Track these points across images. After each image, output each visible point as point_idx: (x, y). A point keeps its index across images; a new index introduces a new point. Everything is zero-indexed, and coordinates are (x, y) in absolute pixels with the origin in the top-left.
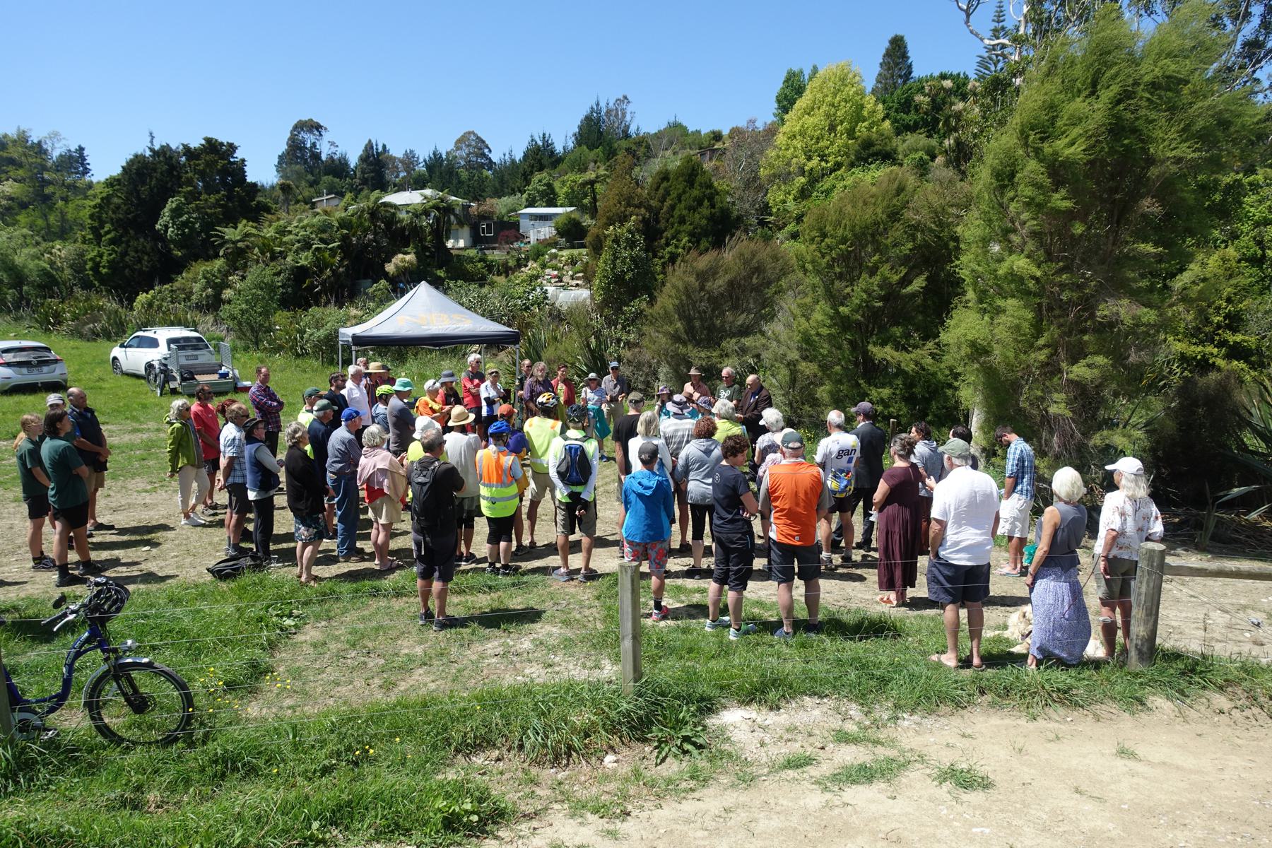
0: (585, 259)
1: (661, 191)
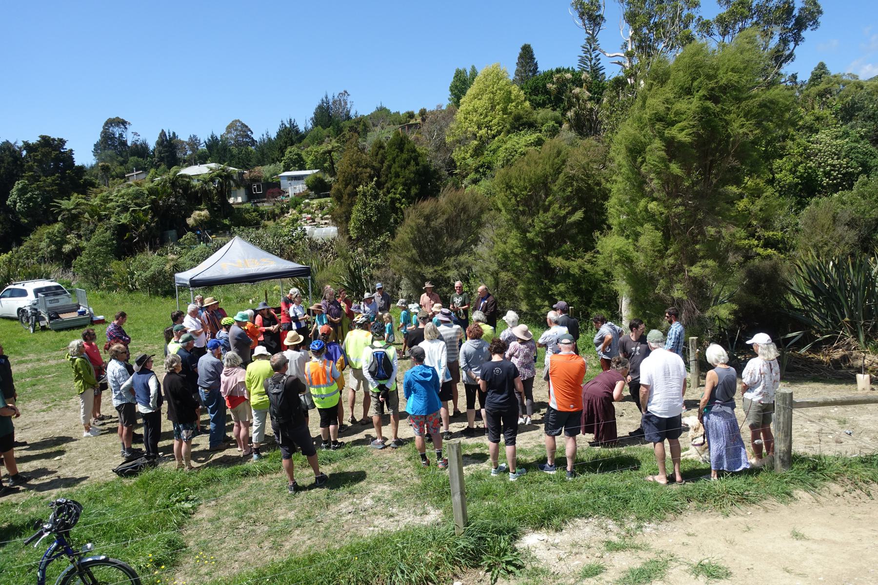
0: (330, 205)
1: (380, 156)
